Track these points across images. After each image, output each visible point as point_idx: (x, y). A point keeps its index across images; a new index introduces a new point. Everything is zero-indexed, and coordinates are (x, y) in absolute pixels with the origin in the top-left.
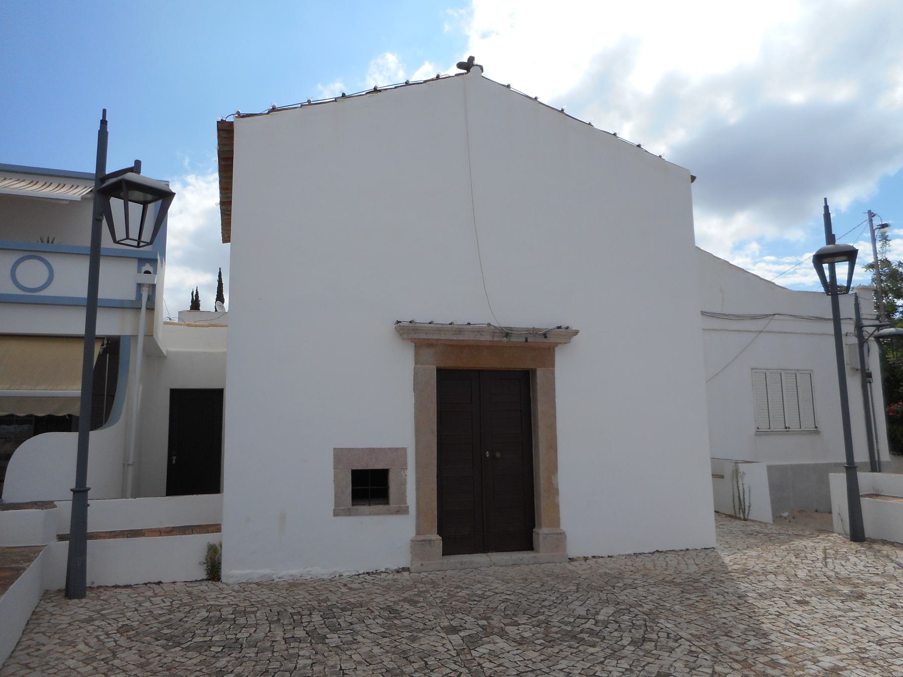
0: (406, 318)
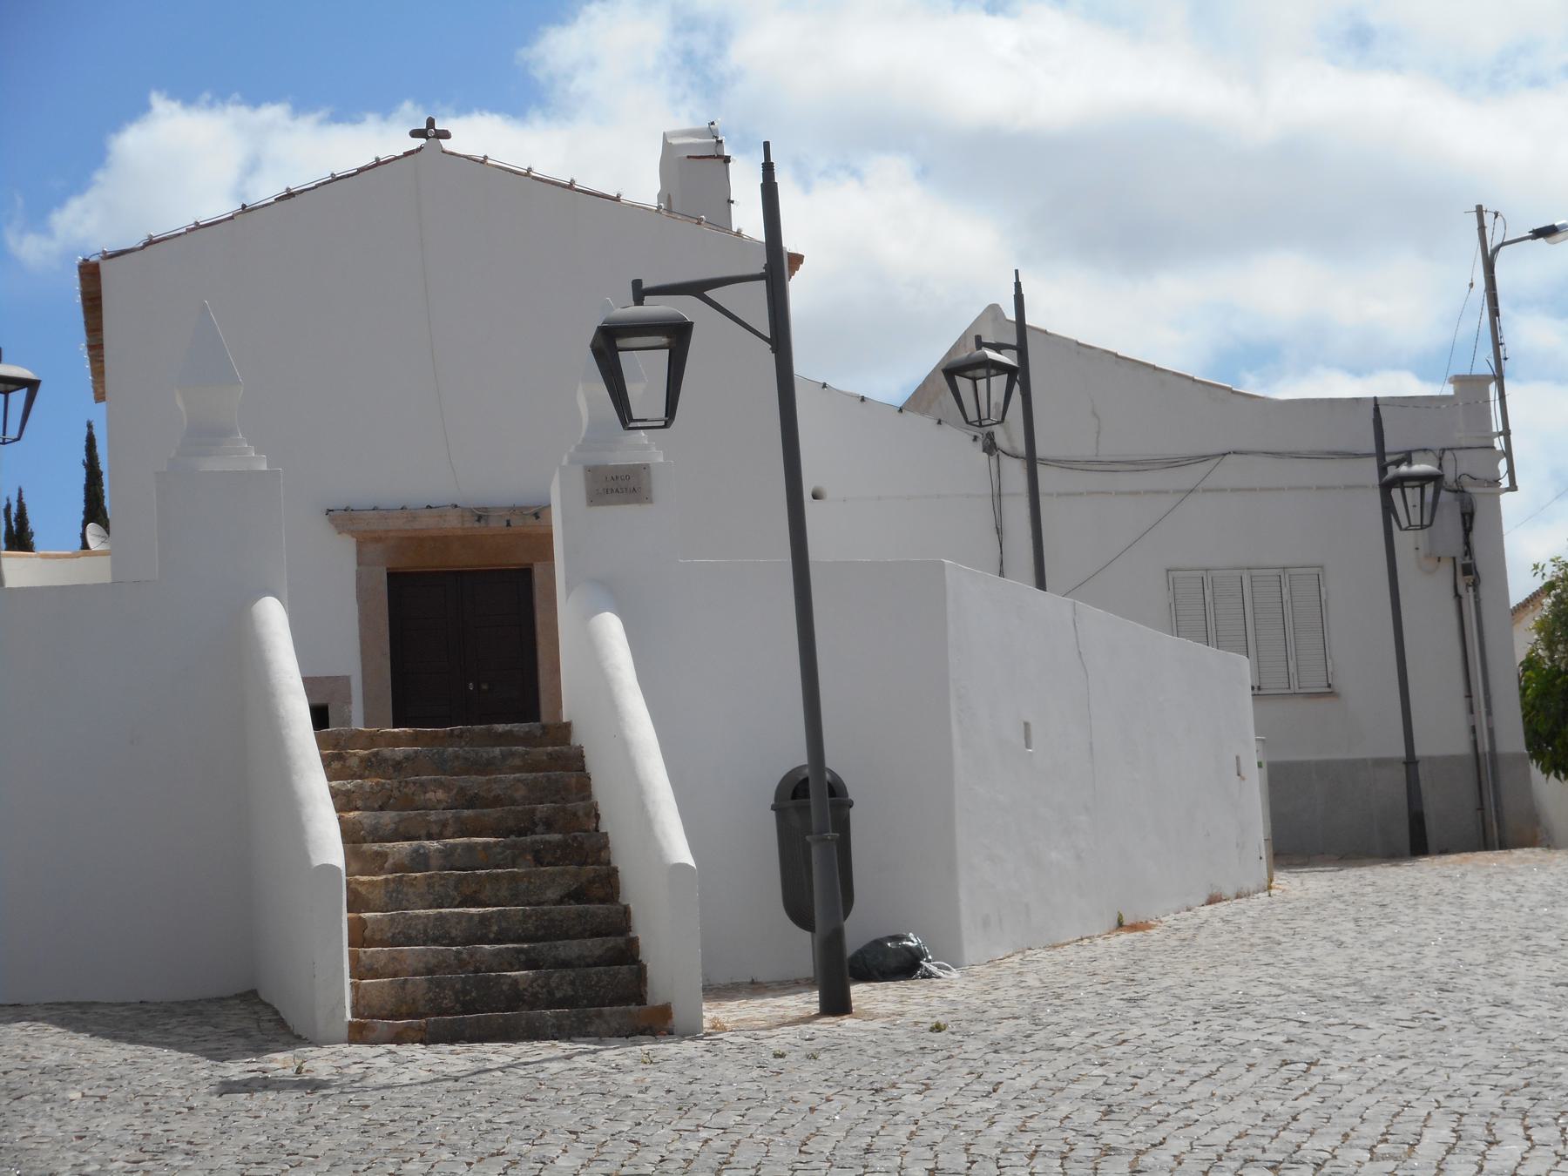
0: (339, 502)
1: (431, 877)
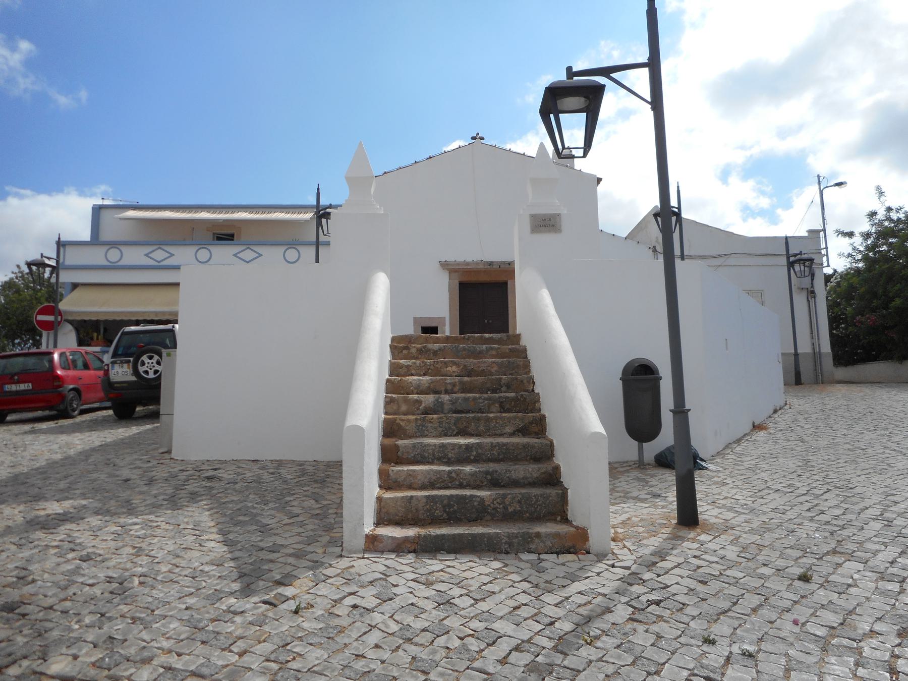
0: (443, 260)
1: (441, 418)
